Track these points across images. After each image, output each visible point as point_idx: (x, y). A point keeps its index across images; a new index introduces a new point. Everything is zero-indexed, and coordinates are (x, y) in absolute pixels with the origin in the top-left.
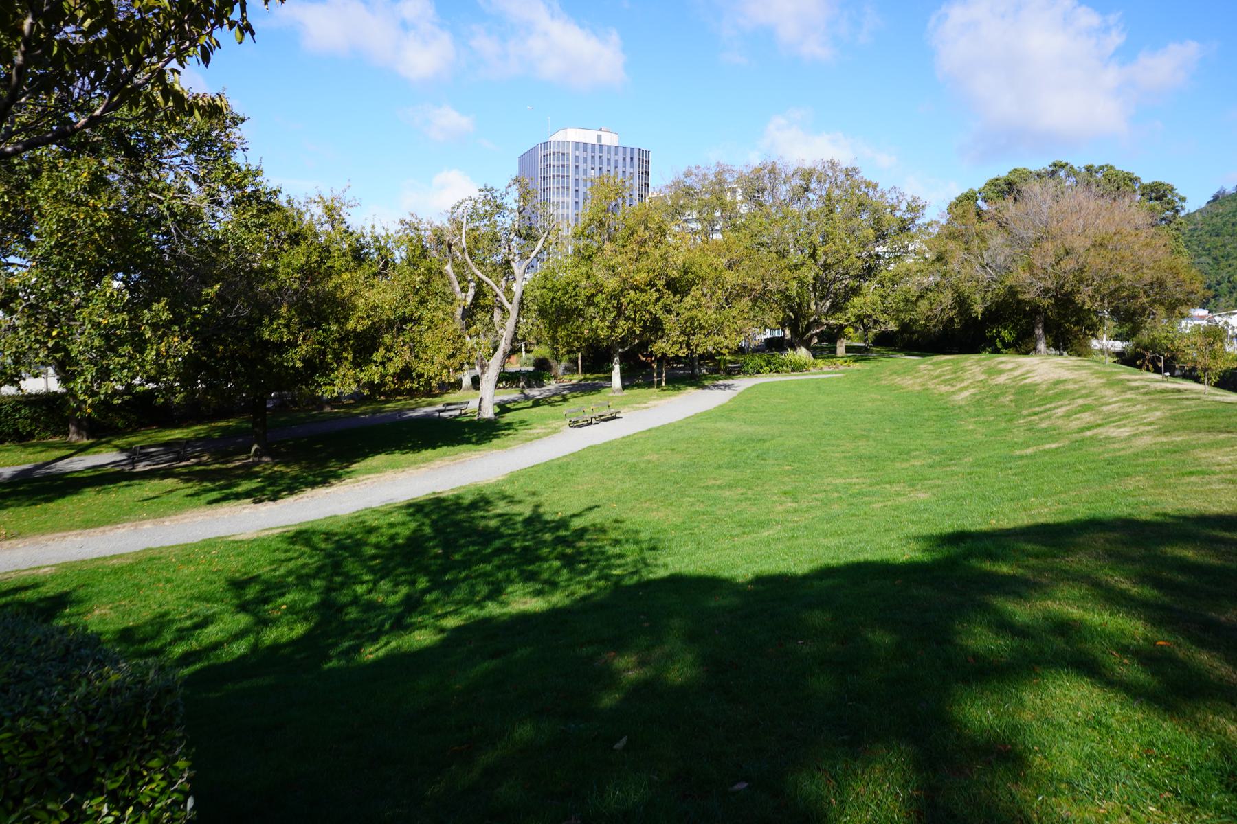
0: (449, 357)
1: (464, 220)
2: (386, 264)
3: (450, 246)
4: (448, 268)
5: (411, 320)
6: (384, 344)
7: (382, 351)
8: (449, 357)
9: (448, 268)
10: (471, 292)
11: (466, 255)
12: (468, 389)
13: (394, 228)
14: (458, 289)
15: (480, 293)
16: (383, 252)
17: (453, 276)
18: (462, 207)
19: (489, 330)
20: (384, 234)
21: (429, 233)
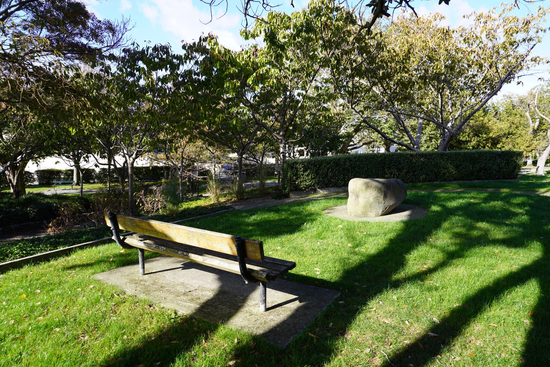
0: (527, 147)
1: (537, 94)
2: (497, 113)
3: (529, 105)
4: (527, 114)
5: (511, 134)
6: (502, 142)
7: (501, 144)
8: (527, 147)
9: (527, 114)
10: (537, 123)
11: (536, 108)
12: (530, 165)
13: (526, 94)
14: (531, 122)
15: (541, 123)
16: (496, 108)
17: (529, 117)
18: (536, 88)
19: (544, 139)
20: (496, 102)
21: (517, 99)
